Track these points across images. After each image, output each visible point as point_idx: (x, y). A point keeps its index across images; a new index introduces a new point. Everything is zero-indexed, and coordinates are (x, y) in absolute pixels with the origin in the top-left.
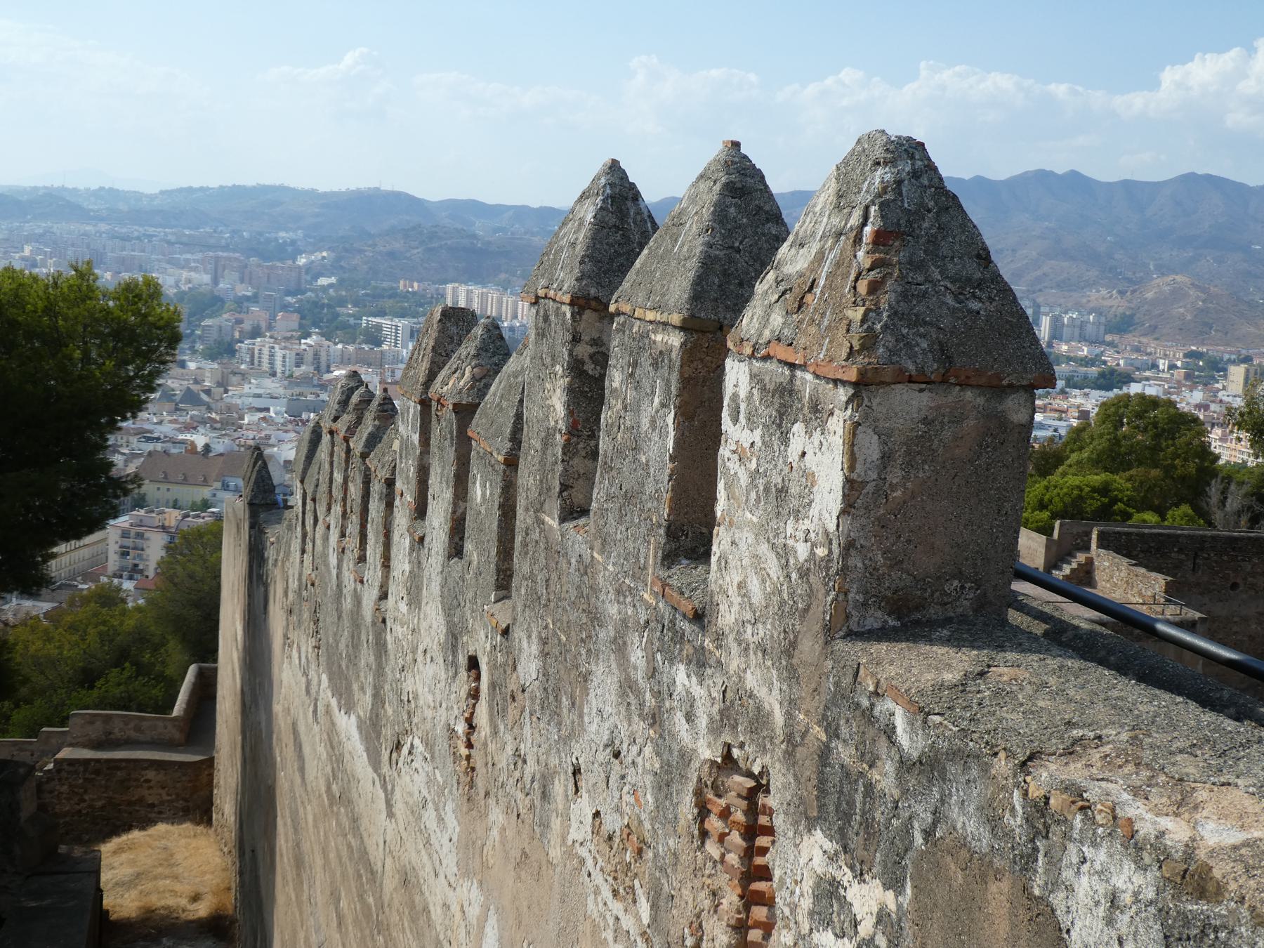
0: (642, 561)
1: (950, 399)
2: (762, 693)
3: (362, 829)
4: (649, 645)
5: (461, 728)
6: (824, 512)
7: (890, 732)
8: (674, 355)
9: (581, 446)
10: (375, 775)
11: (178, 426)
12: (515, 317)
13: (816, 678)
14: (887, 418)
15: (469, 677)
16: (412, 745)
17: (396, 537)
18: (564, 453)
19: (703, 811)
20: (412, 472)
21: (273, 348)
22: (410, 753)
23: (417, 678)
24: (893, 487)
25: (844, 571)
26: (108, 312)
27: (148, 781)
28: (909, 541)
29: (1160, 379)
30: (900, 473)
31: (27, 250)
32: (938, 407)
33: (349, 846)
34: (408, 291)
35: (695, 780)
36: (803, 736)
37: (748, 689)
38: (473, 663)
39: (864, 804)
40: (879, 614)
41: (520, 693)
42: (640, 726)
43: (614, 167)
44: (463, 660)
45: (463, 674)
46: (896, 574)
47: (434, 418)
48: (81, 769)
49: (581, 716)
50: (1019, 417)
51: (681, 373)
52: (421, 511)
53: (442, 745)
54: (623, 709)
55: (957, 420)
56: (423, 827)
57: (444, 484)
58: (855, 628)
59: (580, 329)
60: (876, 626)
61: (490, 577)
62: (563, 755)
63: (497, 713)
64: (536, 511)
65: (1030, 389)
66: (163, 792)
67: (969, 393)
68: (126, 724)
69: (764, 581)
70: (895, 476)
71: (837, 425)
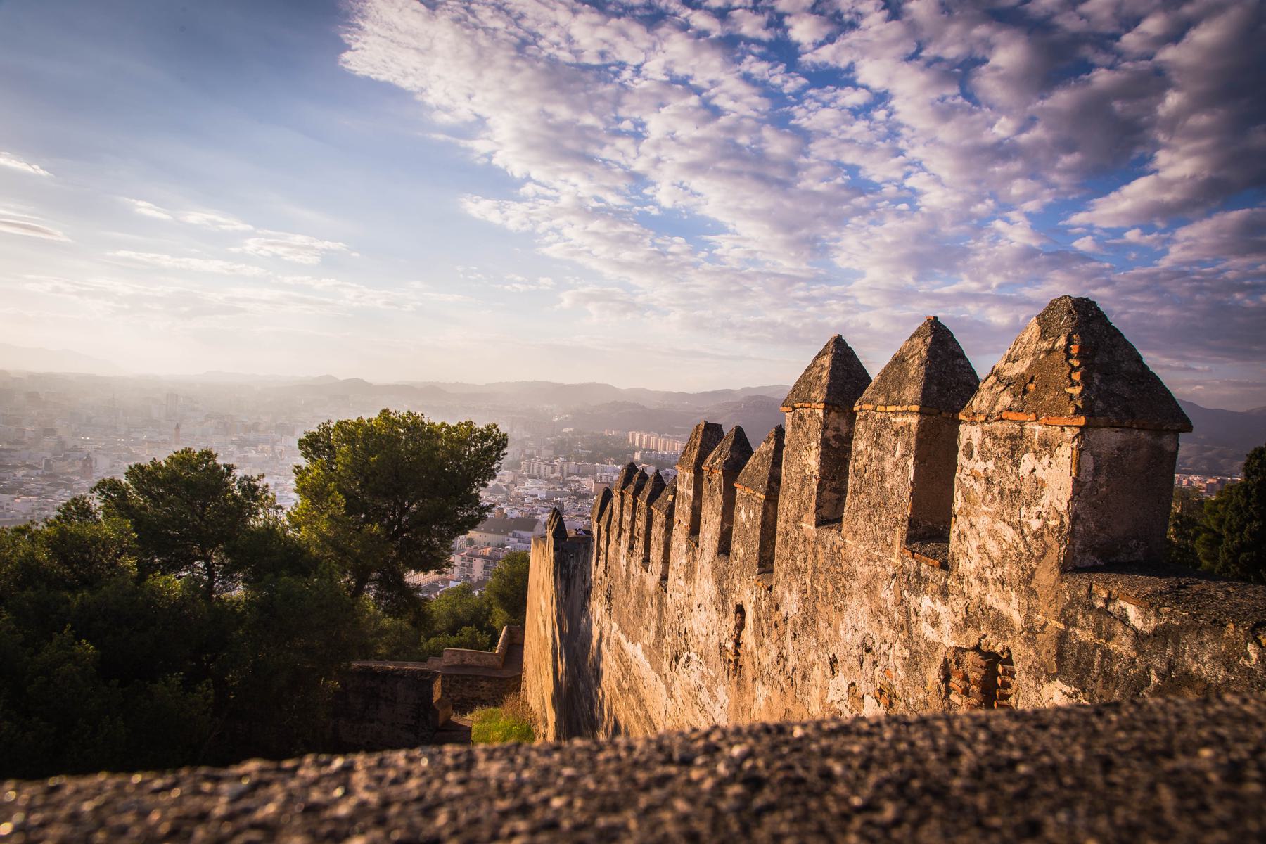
0: (890, 541)
1: (1133, 437)
2: (1001, 606)
3: (647, 705)
4: (897, 587)
5: (730, 645)
6: (1055, 501)
7: (1124, 619)
8: (912, 428)
9: (828, 485)
10: (657, 676)
12: (674, 449)
13: (1054, 593)
14: (1098, 446)
15: (736, 616)
16: (689, 657)
17: (674, 545)
18: (818, 489)
19: (946, 676)
20: (688, 510)
22: (686, 661)
23: (693, 620)
24: (1101, 486)
25: (1072, 533)
26: (39, 563)
27: (482, 687)
28: (1109, 517)
29: (694, 591)
30: (1105, 478)
32: (1126, 442)
33: (636, 715)
35: (942, 659)
36: (1042, 628)
37: (988, 604)
38: (740, 610)
39: (1103, 662)
40: (1092, 557)
41: (782, 622)
42: (889, 633)
44: (731, 607)
45: (732, 615)
46: (1102, 535)
47: (706, 481)
48: (448, 679)
49: (837, 631)
50: (1170, 448)
51: (917, 437)
52: (694, 531)
53: (714, 655)
54: (875, 624)
55: (1137, 449)
56: (699, 701)
57: (714, 514)
58: (1078, 565)
59: (828, 422)
60: (1090, 564)
61: (754, 559)
62: (821, 653)
63: (759, 634)
64: (795, 522)
65: (1177, 432)
66: (489, 693)
67: (1143, 434)
68: (472, 656)
69: (1000, 543)
70: (1102, 479)
71: (1066, 453)
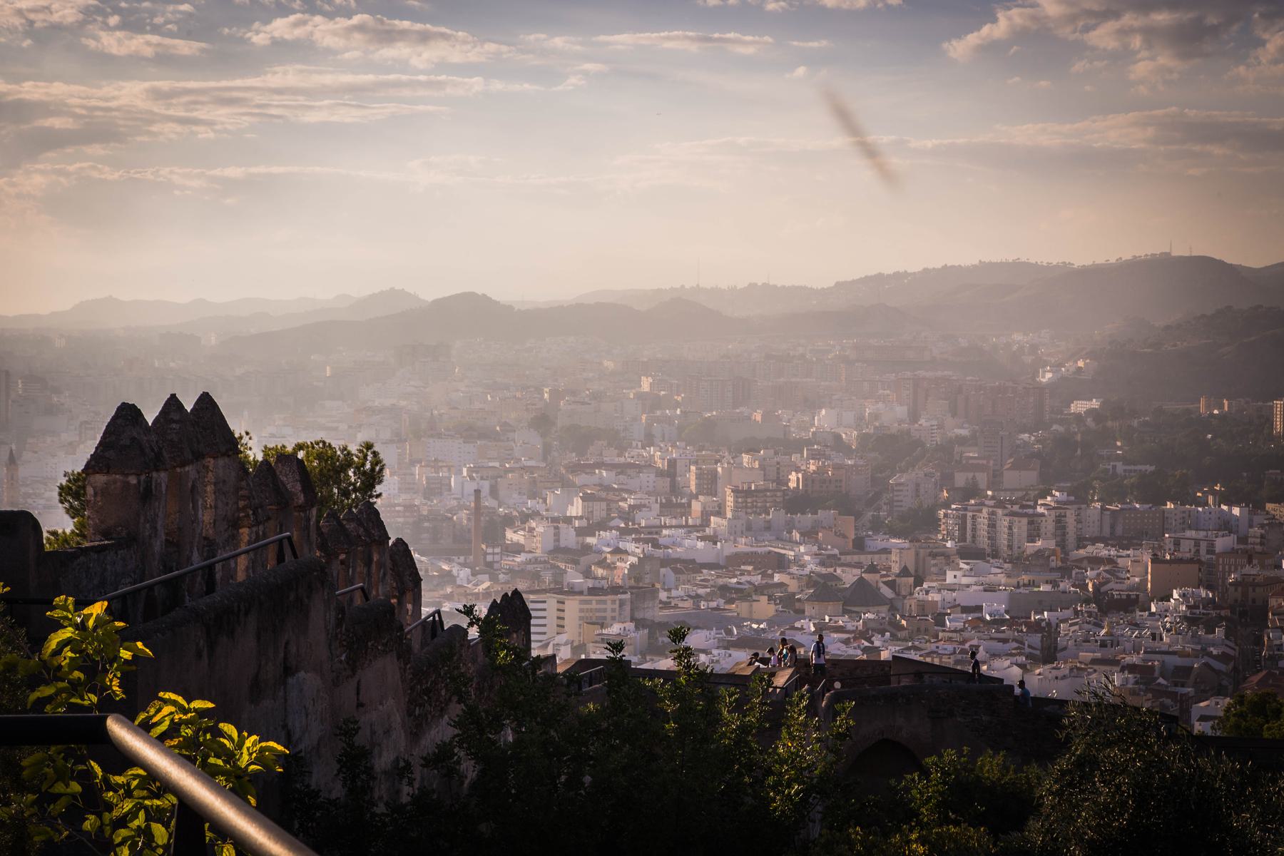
11: (845, 636)
21: (993, 513)
31: (646, 384)
34: (1212, 415)
43: (173, 396)
